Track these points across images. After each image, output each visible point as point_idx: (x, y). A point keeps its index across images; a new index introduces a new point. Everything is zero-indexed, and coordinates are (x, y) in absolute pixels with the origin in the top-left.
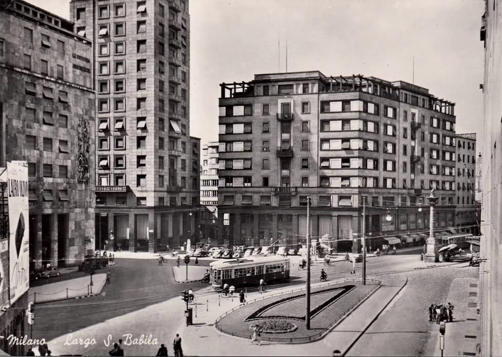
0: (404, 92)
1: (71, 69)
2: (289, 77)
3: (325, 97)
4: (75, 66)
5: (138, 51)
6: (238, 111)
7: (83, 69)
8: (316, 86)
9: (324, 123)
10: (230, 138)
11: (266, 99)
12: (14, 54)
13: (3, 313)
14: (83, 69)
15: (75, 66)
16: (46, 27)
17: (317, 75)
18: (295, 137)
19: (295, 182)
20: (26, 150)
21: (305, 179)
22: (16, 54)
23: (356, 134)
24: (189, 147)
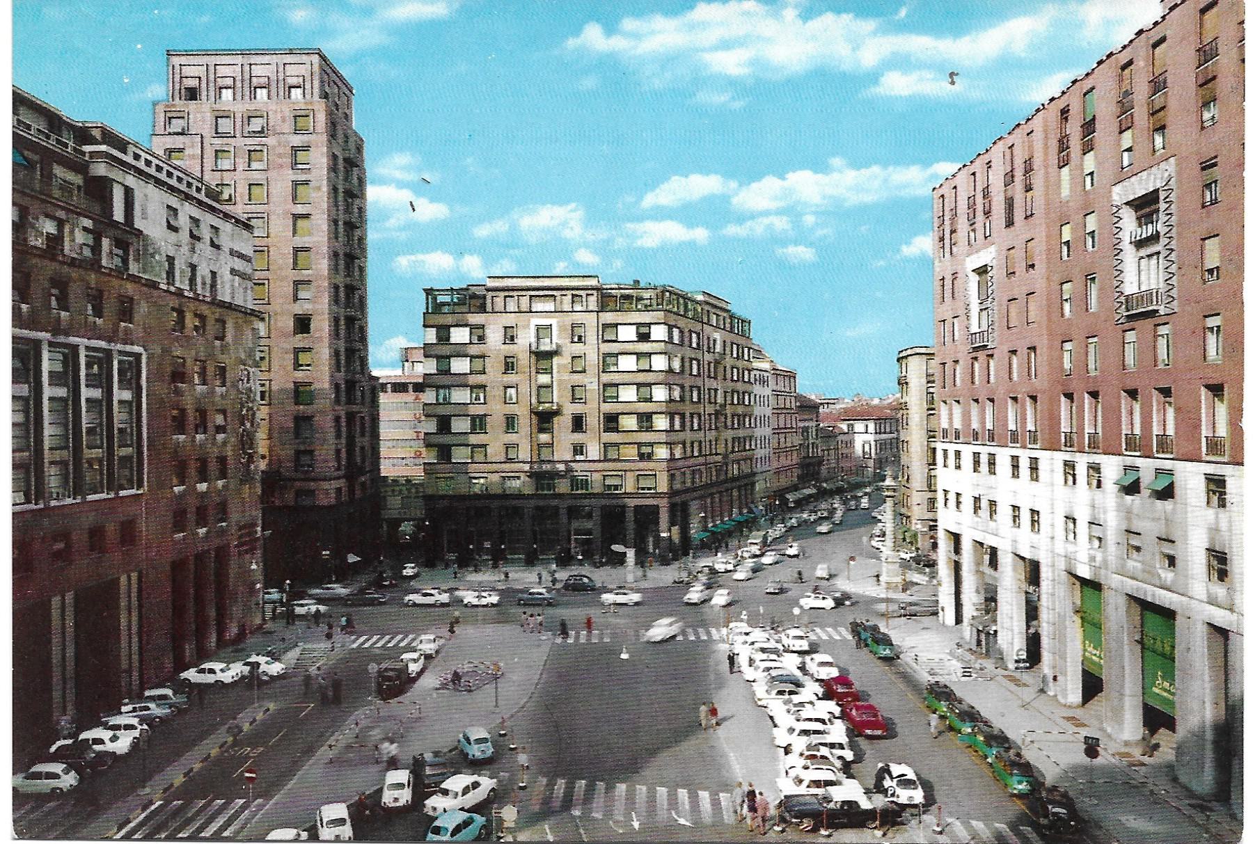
0: (707, 308)
1: (227, 276)
2: (547, 283)
3: (608, 317)
4: (233, 272)
5: (295, 232)
6: (459, 335)
7: (243, 276)
8: (593, 299)
9: (608, 360)
10: (446, 380)
11: (509, 320)
12: (153, 256)
13: (443, 786)
14: (243, 276)
15: (233, 272)
16: (152, 181)
17: (593, 282)
18: (560, 381)
19: (563, 453)
20: (818, 630)
21: (578, 449)
22: (157, 257)
23: (661, 377)
24: (1062, 594)
